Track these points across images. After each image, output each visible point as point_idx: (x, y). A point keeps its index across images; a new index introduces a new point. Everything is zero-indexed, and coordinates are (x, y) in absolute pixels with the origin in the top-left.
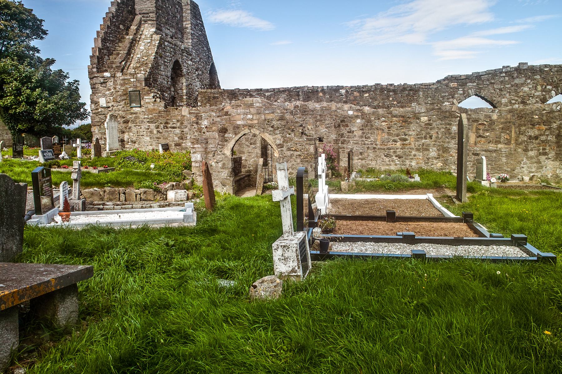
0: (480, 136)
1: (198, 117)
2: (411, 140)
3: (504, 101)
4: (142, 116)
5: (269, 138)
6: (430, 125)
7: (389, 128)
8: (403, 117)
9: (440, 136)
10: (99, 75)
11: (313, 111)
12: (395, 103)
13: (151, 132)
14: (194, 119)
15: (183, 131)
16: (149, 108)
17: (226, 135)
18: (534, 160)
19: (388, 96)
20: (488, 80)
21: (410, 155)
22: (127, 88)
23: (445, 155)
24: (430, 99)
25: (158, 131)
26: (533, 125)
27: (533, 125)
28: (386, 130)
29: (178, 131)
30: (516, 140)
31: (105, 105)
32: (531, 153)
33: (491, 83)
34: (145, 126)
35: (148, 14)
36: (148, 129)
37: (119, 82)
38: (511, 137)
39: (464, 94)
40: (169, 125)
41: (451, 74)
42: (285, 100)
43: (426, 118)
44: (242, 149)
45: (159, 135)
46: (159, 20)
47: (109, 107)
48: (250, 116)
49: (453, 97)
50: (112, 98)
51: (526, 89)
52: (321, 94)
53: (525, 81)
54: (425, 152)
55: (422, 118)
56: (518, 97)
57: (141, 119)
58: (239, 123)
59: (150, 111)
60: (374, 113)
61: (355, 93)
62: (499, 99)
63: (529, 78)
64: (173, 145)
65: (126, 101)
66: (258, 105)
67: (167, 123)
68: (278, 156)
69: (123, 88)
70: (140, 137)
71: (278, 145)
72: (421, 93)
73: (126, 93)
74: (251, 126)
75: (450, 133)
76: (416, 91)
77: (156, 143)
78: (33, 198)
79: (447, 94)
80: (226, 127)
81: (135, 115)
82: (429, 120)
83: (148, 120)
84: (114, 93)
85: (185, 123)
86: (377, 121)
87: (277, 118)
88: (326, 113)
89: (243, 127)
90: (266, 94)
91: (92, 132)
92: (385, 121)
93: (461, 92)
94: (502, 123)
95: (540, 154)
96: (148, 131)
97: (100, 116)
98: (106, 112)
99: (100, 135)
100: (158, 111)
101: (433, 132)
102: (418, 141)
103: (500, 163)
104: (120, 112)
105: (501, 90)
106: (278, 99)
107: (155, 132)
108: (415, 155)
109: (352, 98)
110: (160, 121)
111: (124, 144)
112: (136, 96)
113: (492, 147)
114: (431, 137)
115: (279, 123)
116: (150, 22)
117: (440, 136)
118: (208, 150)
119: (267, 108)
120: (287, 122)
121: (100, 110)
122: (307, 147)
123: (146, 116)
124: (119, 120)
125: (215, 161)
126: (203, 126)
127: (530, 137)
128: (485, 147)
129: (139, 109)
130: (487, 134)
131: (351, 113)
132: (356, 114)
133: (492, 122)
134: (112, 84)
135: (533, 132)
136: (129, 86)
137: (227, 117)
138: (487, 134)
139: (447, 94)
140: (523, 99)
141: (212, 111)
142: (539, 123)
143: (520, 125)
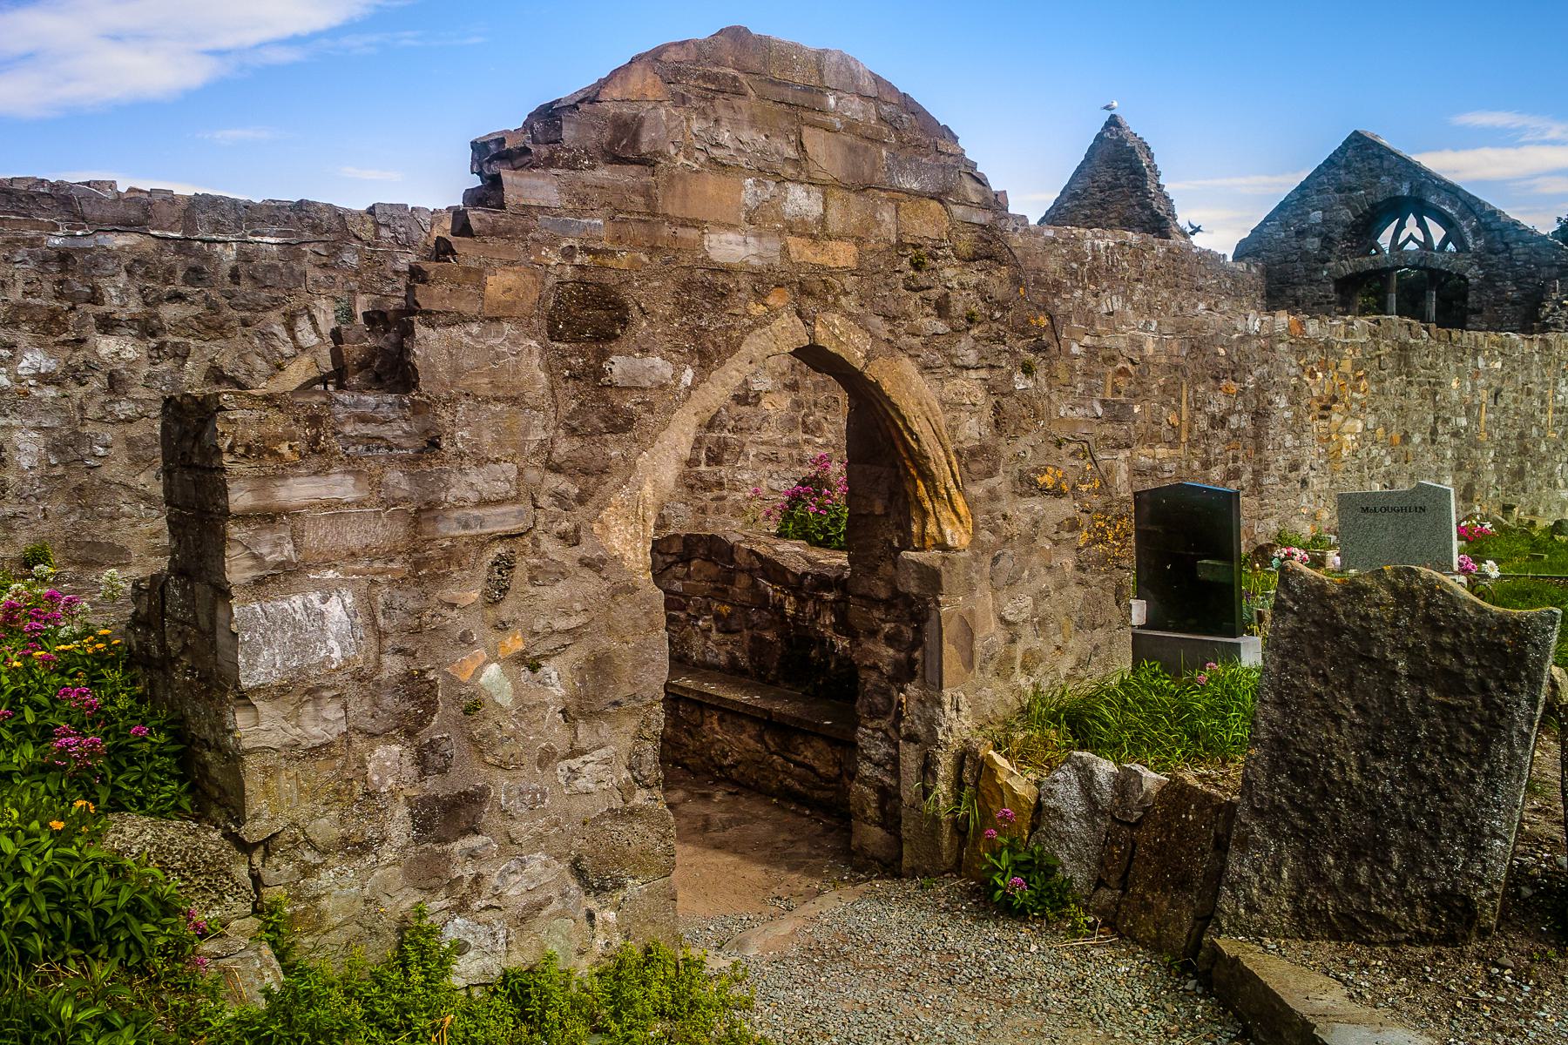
17: (619, 366)
26: (1217, 379)
27: (1217, 379)
38: (1180, 417)
44: (101, 532)
48: (801, 201)
58: (727, 247)
68: (965, 540)
71: (973, 454)
80: (610, 279)
87: (966, 244)
89: (760, 296)
115: (973, 280)
125: (515, 643)
135: (1218, 404)
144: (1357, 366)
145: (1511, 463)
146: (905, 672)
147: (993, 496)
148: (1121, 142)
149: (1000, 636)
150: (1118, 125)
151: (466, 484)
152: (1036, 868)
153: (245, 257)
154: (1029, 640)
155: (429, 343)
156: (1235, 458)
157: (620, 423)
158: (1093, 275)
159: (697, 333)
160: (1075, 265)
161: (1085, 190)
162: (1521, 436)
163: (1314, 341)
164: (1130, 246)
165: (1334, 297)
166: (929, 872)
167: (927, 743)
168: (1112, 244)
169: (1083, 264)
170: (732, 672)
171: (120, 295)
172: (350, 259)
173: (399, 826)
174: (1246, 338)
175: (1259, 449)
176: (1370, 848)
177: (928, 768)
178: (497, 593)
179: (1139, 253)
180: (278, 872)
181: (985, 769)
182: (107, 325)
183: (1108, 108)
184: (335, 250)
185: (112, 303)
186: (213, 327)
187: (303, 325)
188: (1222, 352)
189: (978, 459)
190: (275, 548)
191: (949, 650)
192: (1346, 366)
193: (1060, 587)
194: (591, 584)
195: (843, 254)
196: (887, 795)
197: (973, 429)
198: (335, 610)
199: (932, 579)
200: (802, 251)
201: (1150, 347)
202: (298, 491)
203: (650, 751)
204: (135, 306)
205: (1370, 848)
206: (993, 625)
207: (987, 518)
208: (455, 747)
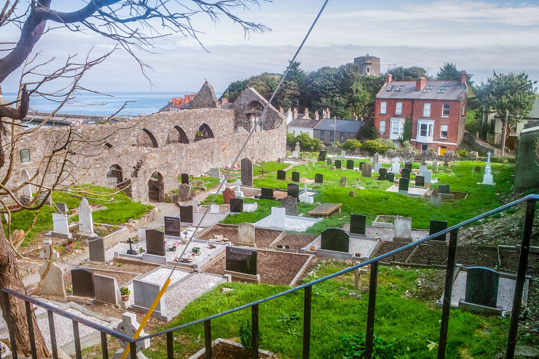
32: (205, 161)
42: (42, 138)
44: (97, 180)
46: (191, 132)
48: (155, 163)
51: (163, 125)
58: (151, 167)
66: (158, 157)
74: (156, 168)
101: (176, 157)
105: (154, 125)
106: (37, 138)
112: (26, 153)
113: (194, 161)
119: (161, 159)
123: (34, 167)
127: (205, 155)
129: (28, 163)
131: (146, 151)
133: (194, 150)
135: (205, 152)
143: (202, 150)
144: (229, 143)
145: (262, 152)
146: (162, 189)
148: (208, 87)
152: (170, 200)
154: (170, 187)
157: (146, 177)
158: (199, 118)
162: (264, 147)
163: (221, 141)
165: (246, 117)
166: (164, 201)
167: (163, 193)
175: (212, 157)
176: (183, 197)
179: (208, 112)
189: (166, 176)
192: (227, 144)
195: (157, 166)
196: (161, 197)
197: (166, 174)
199: (163, 183)
200: (155, 166)
201: (195, 147)
205: (183, 197)
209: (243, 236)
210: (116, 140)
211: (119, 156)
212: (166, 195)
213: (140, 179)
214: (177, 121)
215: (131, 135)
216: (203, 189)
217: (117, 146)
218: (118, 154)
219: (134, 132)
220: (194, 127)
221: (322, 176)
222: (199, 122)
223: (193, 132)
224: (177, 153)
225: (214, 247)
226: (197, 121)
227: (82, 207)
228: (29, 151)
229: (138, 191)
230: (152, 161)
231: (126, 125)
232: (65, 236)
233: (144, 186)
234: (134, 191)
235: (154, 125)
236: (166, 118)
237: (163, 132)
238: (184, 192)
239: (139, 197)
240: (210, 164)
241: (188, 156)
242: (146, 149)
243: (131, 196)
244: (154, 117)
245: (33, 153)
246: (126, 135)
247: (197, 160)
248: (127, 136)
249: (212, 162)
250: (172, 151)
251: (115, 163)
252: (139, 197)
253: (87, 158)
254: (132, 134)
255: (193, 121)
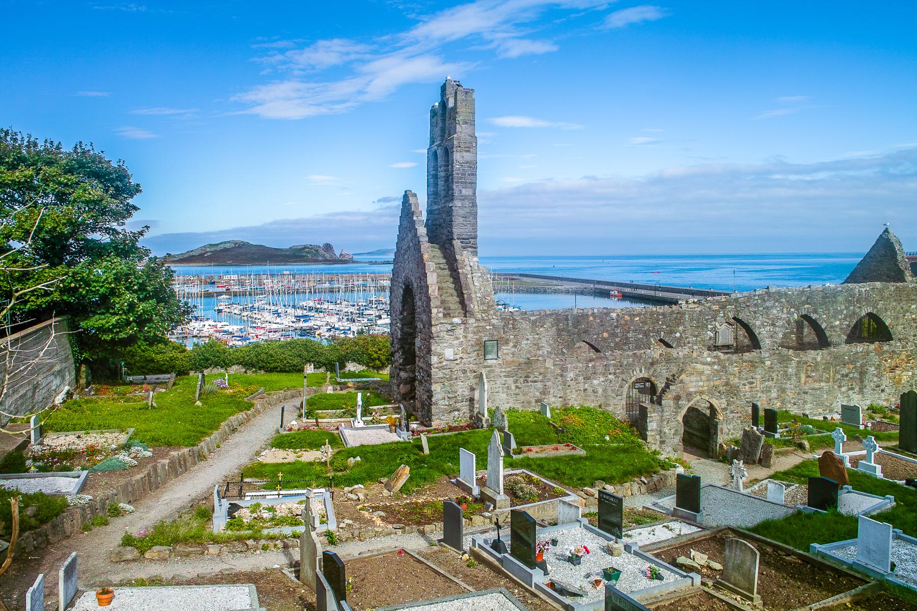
0: (809, 376)
1: (564, 369)
2: (757, 383)
3: (758, 323)
4: (498, 370)
5: (715, 402)
6: (772, 368)
7: (739, 373)
8: (751, 362)
9: (779, 378)
10: (446, 321)
11: (676, 359)
12: (664, 327)
13: (508, 388)
14: (559, 371)
15: (546, 386)
16: (507, 359)
17: (680, 402)
18: (845, 395)
19: (658, 320)
20: (744, 303)
21: (757, 397)
22: (481, 337)
23: (783, 396)
24: (695, 322)
25: (517, 387)
26: (845, 365)
27: (845, 365)
28: (737, 375)
29: (539, 385)
30: (834, 379)
31: (452, 358)
32: (843, 389)
33: (747, 306)
34: (500, 381)
35: (468, 239)
36: (505, 384)
37: (470, 329)
38: (830, 375)
39: (724, 316)
40: (530, 379)
41: (385, 196)
42: (552, 324)
43: (769, 362)
44: (608, 402)
45: (517, 391)
47: (457, 360)
48: (701, 383)
49: (715, 320)
50: (460, 349)
51: (775, 312)
52: (591, 318)
53: (774, 304)
54: (768, 394)
55: (766, 362)
56: (769, 319)
57: (496, 373)
58: (692, 390)
59: (509, 364)
60: (728, 360)
61: (626, 317)
62: (754, 322)
63: (777, 301)
64: (533, 401)
65: (480, 352)
67: (527, 377)
69: (477, 337)
70: (495, 394)
72: (687, 316)
73: (479, 343)
74: (701, 393)
75: (787, 375)
76: (683, 314)
77: (514, 400)
78: (701, 494)
79: (710, 317)
81: (489, 369)
82: (772, 364)
83: (504, 374)
84: (464, 343)
85: (549, 376)
86: (730, 366)
87: (723, 384)
88: (687, 361)
90: (532, 319)
91: (432, 391)
92: (736, 367)
93: (722, 315)
94: (824, 364)
95: (850, 389)
96: (505, 386)
97: (444, 371)
98: (452, 366)
99: (443, 394)
100: (518, 363)
101: (774, 375)
102: (763, 383)
103: (822, 399)
104: (471, 365)
105: (755, 312)
106: (544, 324)
107: (513, 387)
108: (760, 397)
109: (623, 322)
110: (520, 375)
111: (473, 404)
112: (493, 346)
113: (817, 385)
114: (773, 379)
116: (470, 249)
117: (779, 378)
118: (664, 418)
120: (731, 387)
121: (444, 364)
122: (746, 408)
123: (503, 370)
124: (469, 374)
125: (669, 428)
126: (569, 379)
127: (843, 376)
128: (812, 386)
129: (494, 361)
130: (814, 374)
132: (713, 360)
133: (817, 364)
134: (461, 332)
135: (845, 371)
136: (483, 335)
137: (681, 385)
138: (814, 374)
139: (710, 317)
140: (773, 321)
141: (579, 362)
142: (848, 363)
143: (836, 365)
144: (907, 356)
147: (726, 413)
148: (888, 240)
149: (727, 431)
150: (888, 232)
151: (665, 414)
153: (627, 363)
154: (732, 431)
155: (663, 402)
156: (852, 385)
157: (680, 408)
159: (688, 399)
160: (850, 298)
161: (874, 256)
164: (877, 289)
168: (868, 289)
169: (854, 298)
170: (698, 430)
171: (612, 370)
172: (642, 361)
173: (658, 443)
174: (857, 353)
175: (862, 382)
177: (716, 445)
178: (668, 423)
179: (881, 291)
180: (649, 445)
181: (723, 446)
182: (610, 374)
183: (885, 225)
184: (640, 360)
185: (611, 371)
186: (623, 373)
187: (635, 371)
188: (847, 358)
189: (725, 409)
190: (651, 419)
191: (719, 432)
192: (903, 357)
193: (738, 425)
194: (676, 423)
195: (706, 388)
197: (723, 406)
198: (655, 424)
199: (717, 423)
202: (653, 415)
203: (681, 439)
204: (613, 371)
205: (748, 456)
206: (726, 429)
207: (726, 416)
208: (663, 436)
209: (733, 570)
210: (678, 335)
211: (652, 364)
212: (721, 446)
213: (665, 409)
214: (806, 306)
215: (707, 328)
216: (801, 447)
217: (678, 345)
218: (650, 360)
219: (713, 323)
220: (845, 319)
221: (696, 480)
222: (858, 310)
223: (841, 329)
224: (777, 367)
225: (659, 577)
226: (852, 308)
227: (492, 446)
228: (498, 344)
229: (661, 431)
230: (693, 378)
231: (699, 309)
232: (469, 490)
233: (673, 424)
234: (652, 430)
235: (755, 312)
236: (783, 300)
237: (773, 325)
238: (750, 445)
239: (662, 442)
240: (854, 395)
241: (803, 377)
242: (709, 356)
243: (645, 438)
244: (757, 297)
245: (503, 348)
246: (697, 327)
247: (822, 384)
248: (699, 330)
249: (861, 391)
250: (763, 363)
251: (644, 374)
252: (662, 442)
253: (593, 363)
254: (710, 327)
255: (843, 307)
